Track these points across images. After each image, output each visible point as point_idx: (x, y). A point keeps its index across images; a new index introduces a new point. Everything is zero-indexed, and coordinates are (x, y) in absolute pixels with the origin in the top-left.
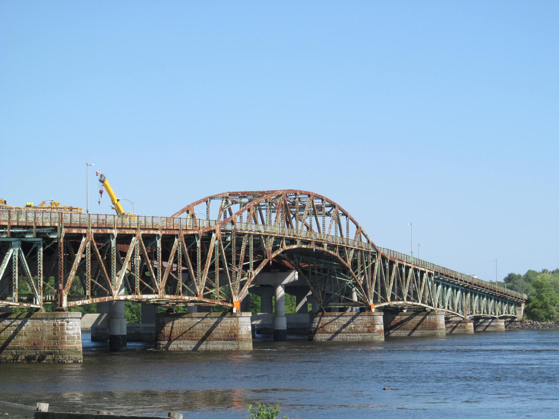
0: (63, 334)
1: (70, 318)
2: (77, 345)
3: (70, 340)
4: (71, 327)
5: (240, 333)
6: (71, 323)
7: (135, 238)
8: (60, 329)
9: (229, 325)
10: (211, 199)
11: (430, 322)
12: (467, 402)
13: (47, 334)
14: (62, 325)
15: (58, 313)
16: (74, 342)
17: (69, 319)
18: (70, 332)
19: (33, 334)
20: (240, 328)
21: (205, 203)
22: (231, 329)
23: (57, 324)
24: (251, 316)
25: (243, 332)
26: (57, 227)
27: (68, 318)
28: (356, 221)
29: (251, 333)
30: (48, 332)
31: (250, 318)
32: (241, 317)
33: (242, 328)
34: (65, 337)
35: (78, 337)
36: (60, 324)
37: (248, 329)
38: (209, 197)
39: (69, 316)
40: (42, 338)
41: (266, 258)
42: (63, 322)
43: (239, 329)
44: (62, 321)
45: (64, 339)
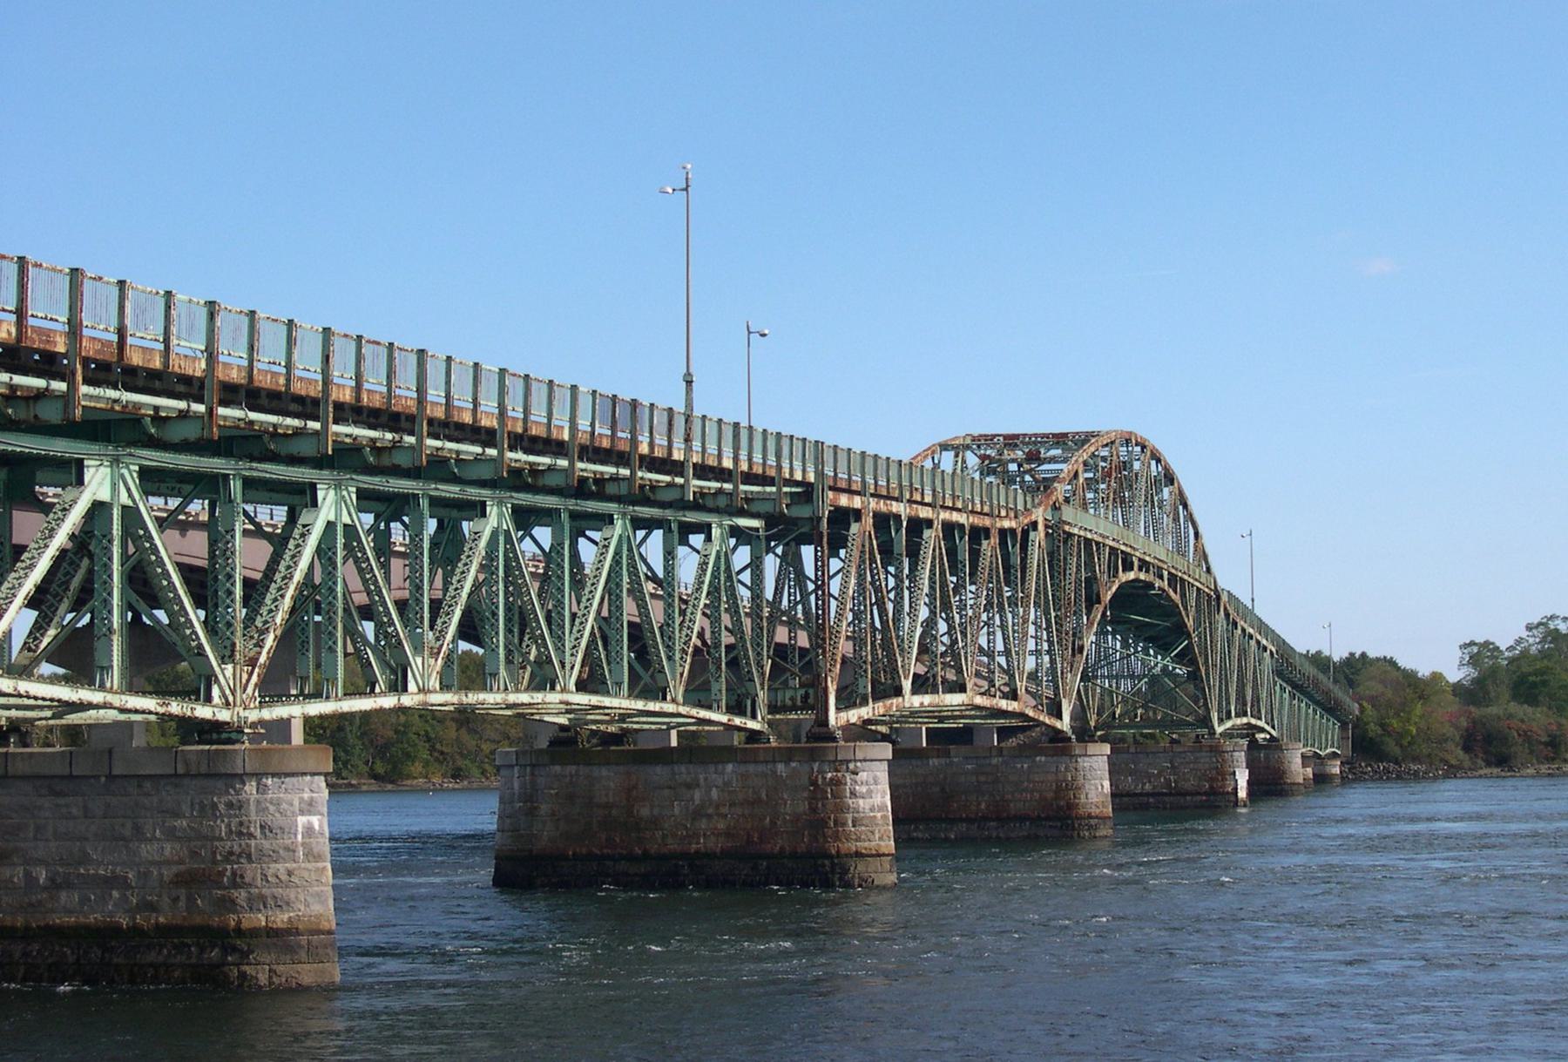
0: (842, 808)
1: (860, 761)
2: (882, 843)
3: (863, 828)
4: (864, 789)
5: (1083, 800)
6: (863, 776)
7: (930, 531)
8: (829, 796)
9: (1051, 777)
10: (946, 450)
11: (1268, 768)
12: (1510, 945)
13: (788, 810)
14: (837, 783)
15: (825, 747)
16: (873, 833)
17: (859, 764)
18: (861, 802)
19: (746, 812)
20: (1083, 785)
21: (952, 453)
22: (1059, 788)
23: (820, 782)
24: (891, 758)
25: (1089, 796)
26: (813, 484)
27: (855, 761)
28: (258, 541)
29: (1109, 799)
30: (793, 805)
31: (885, 765)
32: (1086, 755)
33: (1087, 786)
34: (846, 819)
35: (884, 817)
36: (831, 779)
37: (1102, 786)
38: (940, 445)
39: (859, 755)
40: (773, 823)
41: (1099, 603)
42: (839, 774)
43: (1080, 788)
44: (837, 771)
45: (844, 824)
